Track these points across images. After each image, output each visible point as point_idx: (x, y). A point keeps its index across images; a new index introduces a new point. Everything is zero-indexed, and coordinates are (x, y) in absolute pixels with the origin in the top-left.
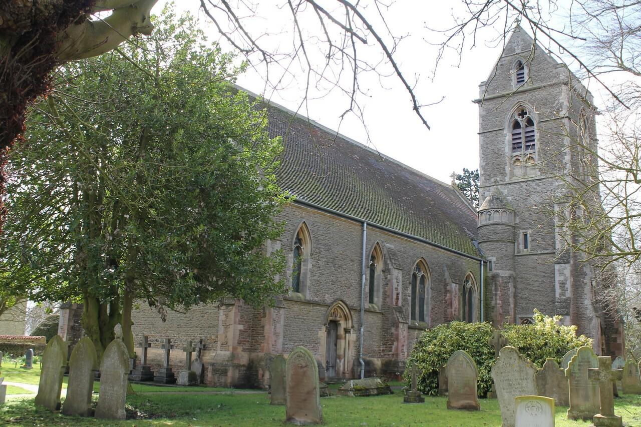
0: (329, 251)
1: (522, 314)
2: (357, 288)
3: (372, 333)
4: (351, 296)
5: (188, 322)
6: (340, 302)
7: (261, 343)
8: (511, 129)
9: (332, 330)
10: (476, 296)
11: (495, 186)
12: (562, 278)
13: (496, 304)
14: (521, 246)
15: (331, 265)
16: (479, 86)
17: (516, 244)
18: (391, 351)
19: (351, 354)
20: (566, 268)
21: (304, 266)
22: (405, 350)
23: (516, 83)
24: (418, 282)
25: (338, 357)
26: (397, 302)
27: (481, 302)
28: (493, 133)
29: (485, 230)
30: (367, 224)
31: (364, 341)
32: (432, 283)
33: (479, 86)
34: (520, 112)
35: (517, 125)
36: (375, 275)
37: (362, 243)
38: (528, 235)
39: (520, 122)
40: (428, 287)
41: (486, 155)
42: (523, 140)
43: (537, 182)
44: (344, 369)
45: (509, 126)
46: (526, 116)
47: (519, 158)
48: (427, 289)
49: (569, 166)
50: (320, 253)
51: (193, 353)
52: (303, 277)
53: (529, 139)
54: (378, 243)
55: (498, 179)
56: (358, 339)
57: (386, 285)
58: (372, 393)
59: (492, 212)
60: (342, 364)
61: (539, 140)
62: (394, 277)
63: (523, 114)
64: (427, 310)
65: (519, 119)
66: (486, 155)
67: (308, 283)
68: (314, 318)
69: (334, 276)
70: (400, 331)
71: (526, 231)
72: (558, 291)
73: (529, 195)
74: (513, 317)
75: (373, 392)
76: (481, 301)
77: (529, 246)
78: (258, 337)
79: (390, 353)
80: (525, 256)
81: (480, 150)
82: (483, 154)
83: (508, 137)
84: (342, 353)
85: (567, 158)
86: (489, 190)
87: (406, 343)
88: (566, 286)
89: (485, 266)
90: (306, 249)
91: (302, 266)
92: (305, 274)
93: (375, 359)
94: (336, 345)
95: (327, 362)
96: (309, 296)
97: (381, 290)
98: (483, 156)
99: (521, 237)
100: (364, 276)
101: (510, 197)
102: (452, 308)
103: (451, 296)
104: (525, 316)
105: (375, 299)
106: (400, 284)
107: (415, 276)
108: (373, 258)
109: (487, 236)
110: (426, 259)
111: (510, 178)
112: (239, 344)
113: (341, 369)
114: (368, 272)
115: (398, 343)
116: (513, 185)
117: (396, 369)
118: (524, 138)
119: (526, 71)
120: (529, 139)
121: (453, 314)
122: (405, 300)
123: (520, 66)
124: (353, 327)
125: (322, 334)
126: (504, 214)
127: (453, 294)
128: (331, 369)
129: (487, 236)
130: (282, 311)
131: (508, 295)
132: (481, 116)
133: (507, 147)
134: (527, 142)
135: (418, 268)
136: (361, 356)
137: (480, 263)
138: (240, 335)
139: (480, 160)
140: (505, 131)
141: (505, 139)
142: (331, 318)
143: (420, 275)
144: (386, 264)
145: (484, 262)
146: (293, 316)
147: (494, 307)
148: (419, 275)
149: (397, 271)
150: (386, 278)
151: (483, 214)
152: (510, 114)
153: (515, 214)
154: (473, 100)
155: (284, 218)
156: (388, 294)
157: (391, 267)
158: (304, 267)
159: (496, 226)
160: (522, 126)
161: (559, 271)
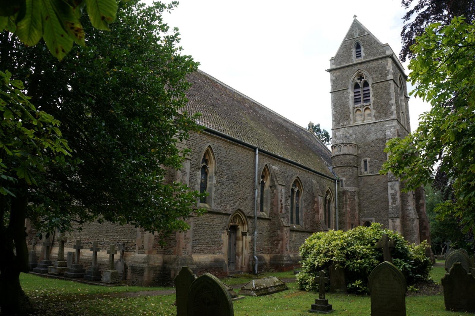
0: (229, 170)
1: (365, 217)
2: (251, 200)
3: (263, 235)
4: (247, 206)
5: (114, 228)
6: (239, 211)
7: (174, 246)
8: (353, 89)
9: (232, 234)
10: (332, 205)
11: (343, 128)
12: (393, 192)
13: (346, 211)
14: (363, 170)
15: (232, 181)
16: (330, 60)
17: (359, 168)
18: (278, 248)
19: (247, 252)
20: (396, 184)
21: (209, 181)
22: (288, 248)
23: (356, 57)
24: (295, 196)
25: (237, 254)
26: (282, 210)
27: (336, 210)
28: (341, 91)
29: (337, 159)
30: (259, 150)
31: (257, 241)
32: (304, 196)
33: (330, 60)
34: (359, 77)
35: (357, 86)
36: (265, 190)
37: (255, 164)
38: (367, 162)
39: (359, 84)
40: (302, 199)
41: (336, 107)
42: (361, 96)
43: (373, 124)
44: (242, 264)
45: (352, 86)
46: (363, 80)
47: (360, 108)
48: (301, 200)
49: (395, 112)
50: (222, 172)
51: (115, 255)
52: (209, 191)
53: (366, 95)
54: (266, 165)
55: (345, 123)
56: (252, 240)
57: (273, 197)
58: (271, 291)
59: (342, 146)
60: (240, 260)
61: (373, 96)
62: (279, 191)
63: (361, 78)
64: (302, 216)
65: (359, 82)
66: (336, 107)
67: (213, 196)
68: (218, 224)
69: (234, 190)
70: (284, 233)
71: (366, 159)
72: (390, 200)
73: (367, 133)
74: (358, 219)
75: (272, 289)
76: (336, 209)
77: (368, 170)
78: (170, 241)
79: (277, 250)
80: (366, 177)
81: (332, 104)
82: (334, 106)
83: (352, 94)
84: (240, 251)
85: (394, 107)
86: (339, 131)
87: (288, 242)
88: (396, 197)
89: (338, 184)
90: (212, 168)
91: (208, 181)
92: (211, 188)
93: (265, 255)
94: (235, 245)
95: (229, 259)
96: (214, 207)
97: (269, 201)
98: (334, 107)
99: (363, 163)
100: (257, 190)
101: (354, 136)
102: (318, 214)
103: (318, 205)
104: (366, 219)
105: (265, 208)
106: (283, 197)
107: (292, 190)
108: (263, 177)
109: (339, 163)
110: (300, 178)
111: (353, 123)
112: (154, 247)
113: (240, 264)
114: (260, 187)
115: (283, 242)
116: (356, 127)
117: (282, 262)
118: (363, 95)
119: (362, 49)
120: (366, 95)
121: (320, 218)
122: (286, 209)
123: (358, 47)
124: (248, 231)
125: (225, 237)
126: (351, 147)
127: (319, 204)
128: (231, 264)
129: (339, 163)
130: (191, 219)
131: (355, 204)
132: (332, 80)
133: (351, 101)
134: (364, 97)
135: (295, 185)
136: (255, 253)
137: (335, 182)
138: (154, 240)
139: (332, 111)
140: (349, 90)
141: (349, 95)
142: (231, 224)
143: (296, 190)
144: (272, 181)
145: (338, 181)
146: (201, 223)
147: (345, 213)
148: (296, 190)
149: (281, 186)
150: (273, 192)
151: (336, 148)
152: (352, 78)
153: (358, 148)
154: (326, 70)
155: (193, 142)
156: (274, 204)
157: (276, 184)
158: (210, 183)
159: (345, 156)
160: (360, 87)
161: (391, 186)
